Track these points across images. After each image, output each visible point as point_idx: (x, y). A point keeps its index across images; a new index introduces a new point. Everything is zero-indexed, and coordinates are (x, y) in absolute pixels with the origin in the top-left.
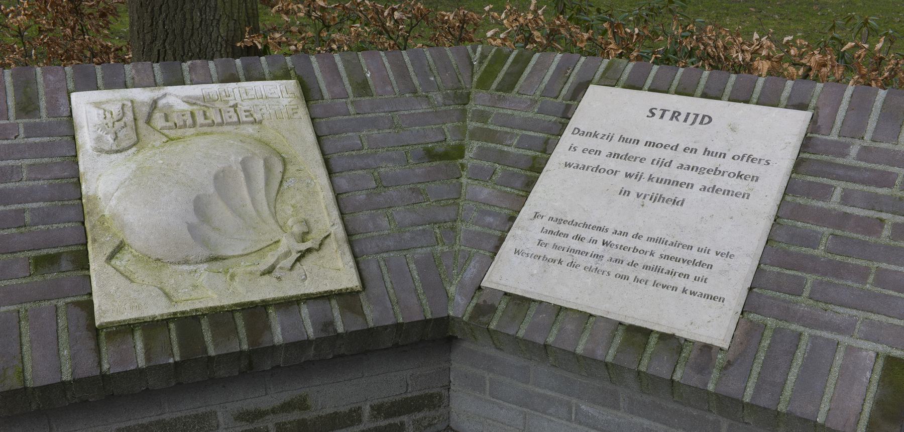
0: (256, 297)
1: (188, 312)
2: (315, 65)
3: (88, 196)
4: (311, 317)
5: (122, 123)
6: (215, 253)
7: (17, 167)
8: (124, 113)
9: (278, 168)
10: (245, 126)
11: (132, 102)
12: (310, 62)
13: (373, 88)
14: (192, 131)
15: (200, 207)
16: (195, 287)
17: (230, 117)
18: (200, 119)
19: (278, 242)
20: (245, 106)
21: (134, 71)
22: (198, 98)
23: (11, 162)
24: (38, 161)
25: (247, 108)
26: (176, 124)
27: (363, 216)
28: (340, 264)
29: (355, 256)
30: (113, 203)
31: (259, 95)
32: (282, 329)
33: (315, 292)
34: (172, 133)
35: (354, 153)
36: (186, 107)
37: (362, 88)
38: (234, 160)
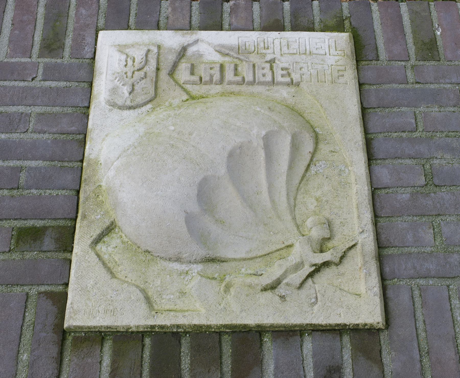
0: (251, 319)
1: (168, 327)
2: (376, 15)
3: (89, 160)
4: (314, 356)
5: (142, 73)
6: (212, 254)
7: (26, 114)
8: (147, 61)
9: (308, 146)
10: (279, 87)
11: (159, 47)
12: (371, 11)
13: (441, 50)
14: (219, 88)
15: (205, 194)
16: (183, 293)
17: (264, 75)
18: (229, 75)
19: (290, 246)
20: (283, 62)
21: (170, 9)
22: (231, 48)
23: (21, 109)
24: (49, 109)
25: (285, 65)
26: (201, 79)
27: (401, 223)
28: (362, 289)
29: (383, 279)
30: (111, 173)
31: (302, 49)
32: (276, 368)
33: (324, 323)
34: (195, 90)
35: (404, 135)
36: (217, 58)
37: (429, 49)
38: (257, 133)
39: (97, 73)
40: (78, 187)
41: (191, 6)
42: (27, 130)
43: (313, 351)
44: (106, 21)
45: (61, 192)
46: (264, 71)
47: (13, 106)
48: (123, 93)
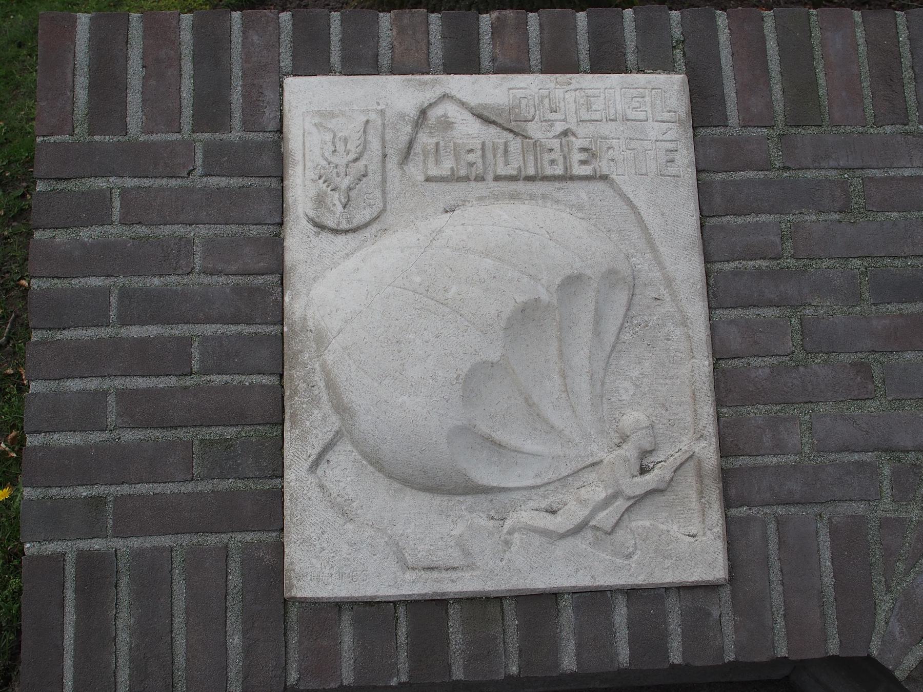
2: (724, 37)
12: (715, 29)
23: (179, 230)
25: (586, 144)
32: (579, 646)
37: (804, 108)
39: (288, 161)
40: (280, 369)
41: (428, 25)
42: (193, 268)
43: (629, 618)
44: (294, 56)
45: (256, 379)
46: (553, 156)
47: (165, 225)
48: (335, 205)
